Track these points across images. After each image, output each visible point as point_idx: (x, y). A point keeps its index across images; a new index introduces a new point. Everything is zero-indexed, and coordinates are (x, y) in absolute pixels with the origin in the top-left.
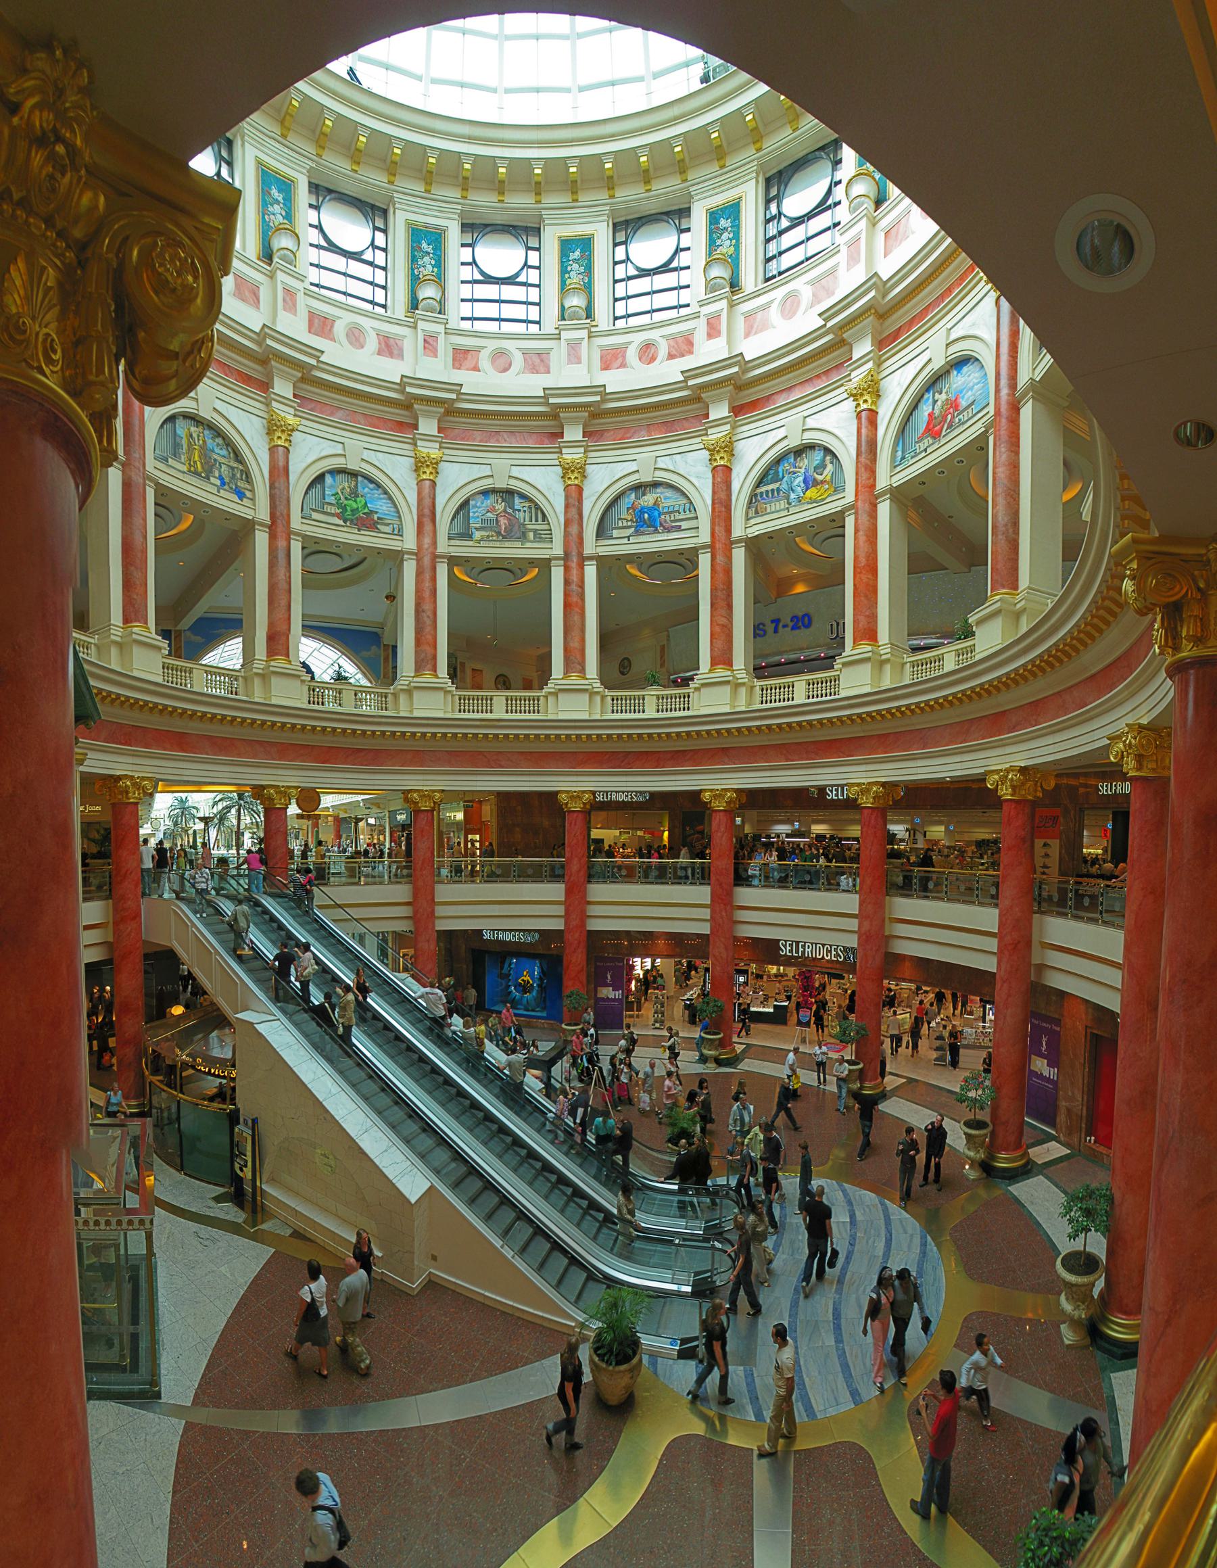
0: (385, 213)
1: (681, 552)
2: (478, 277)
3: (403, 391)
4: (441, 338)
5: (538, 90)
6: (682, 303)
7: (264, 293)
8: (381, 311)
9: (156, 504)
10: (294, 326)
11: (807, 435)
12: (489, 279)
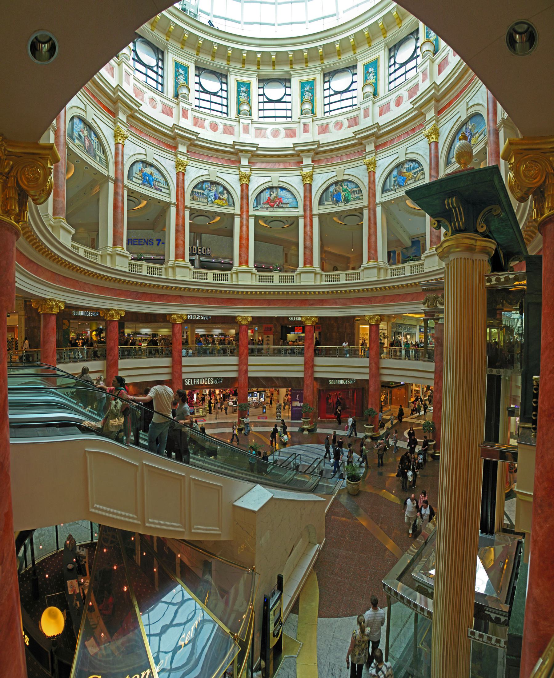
0: (226, 77)
1: (356, 210)
2: (266, 100)
3: (234, 148)
4: (250, 125)
5: (292, 24)
6: (354, 104)
7: (175, 111)
8: (225, 115)
9: (128, 196)
10: (187, 124)
11: (408, 156)
12: (270, 101)
